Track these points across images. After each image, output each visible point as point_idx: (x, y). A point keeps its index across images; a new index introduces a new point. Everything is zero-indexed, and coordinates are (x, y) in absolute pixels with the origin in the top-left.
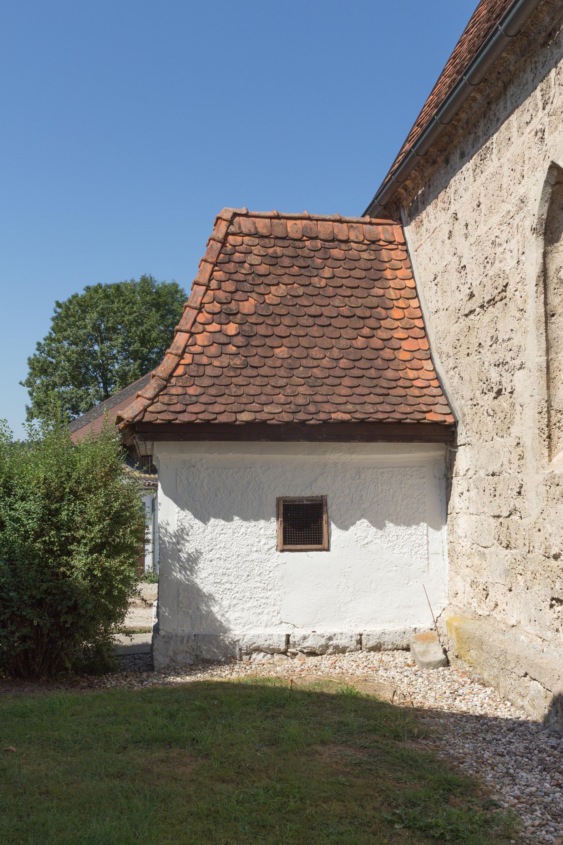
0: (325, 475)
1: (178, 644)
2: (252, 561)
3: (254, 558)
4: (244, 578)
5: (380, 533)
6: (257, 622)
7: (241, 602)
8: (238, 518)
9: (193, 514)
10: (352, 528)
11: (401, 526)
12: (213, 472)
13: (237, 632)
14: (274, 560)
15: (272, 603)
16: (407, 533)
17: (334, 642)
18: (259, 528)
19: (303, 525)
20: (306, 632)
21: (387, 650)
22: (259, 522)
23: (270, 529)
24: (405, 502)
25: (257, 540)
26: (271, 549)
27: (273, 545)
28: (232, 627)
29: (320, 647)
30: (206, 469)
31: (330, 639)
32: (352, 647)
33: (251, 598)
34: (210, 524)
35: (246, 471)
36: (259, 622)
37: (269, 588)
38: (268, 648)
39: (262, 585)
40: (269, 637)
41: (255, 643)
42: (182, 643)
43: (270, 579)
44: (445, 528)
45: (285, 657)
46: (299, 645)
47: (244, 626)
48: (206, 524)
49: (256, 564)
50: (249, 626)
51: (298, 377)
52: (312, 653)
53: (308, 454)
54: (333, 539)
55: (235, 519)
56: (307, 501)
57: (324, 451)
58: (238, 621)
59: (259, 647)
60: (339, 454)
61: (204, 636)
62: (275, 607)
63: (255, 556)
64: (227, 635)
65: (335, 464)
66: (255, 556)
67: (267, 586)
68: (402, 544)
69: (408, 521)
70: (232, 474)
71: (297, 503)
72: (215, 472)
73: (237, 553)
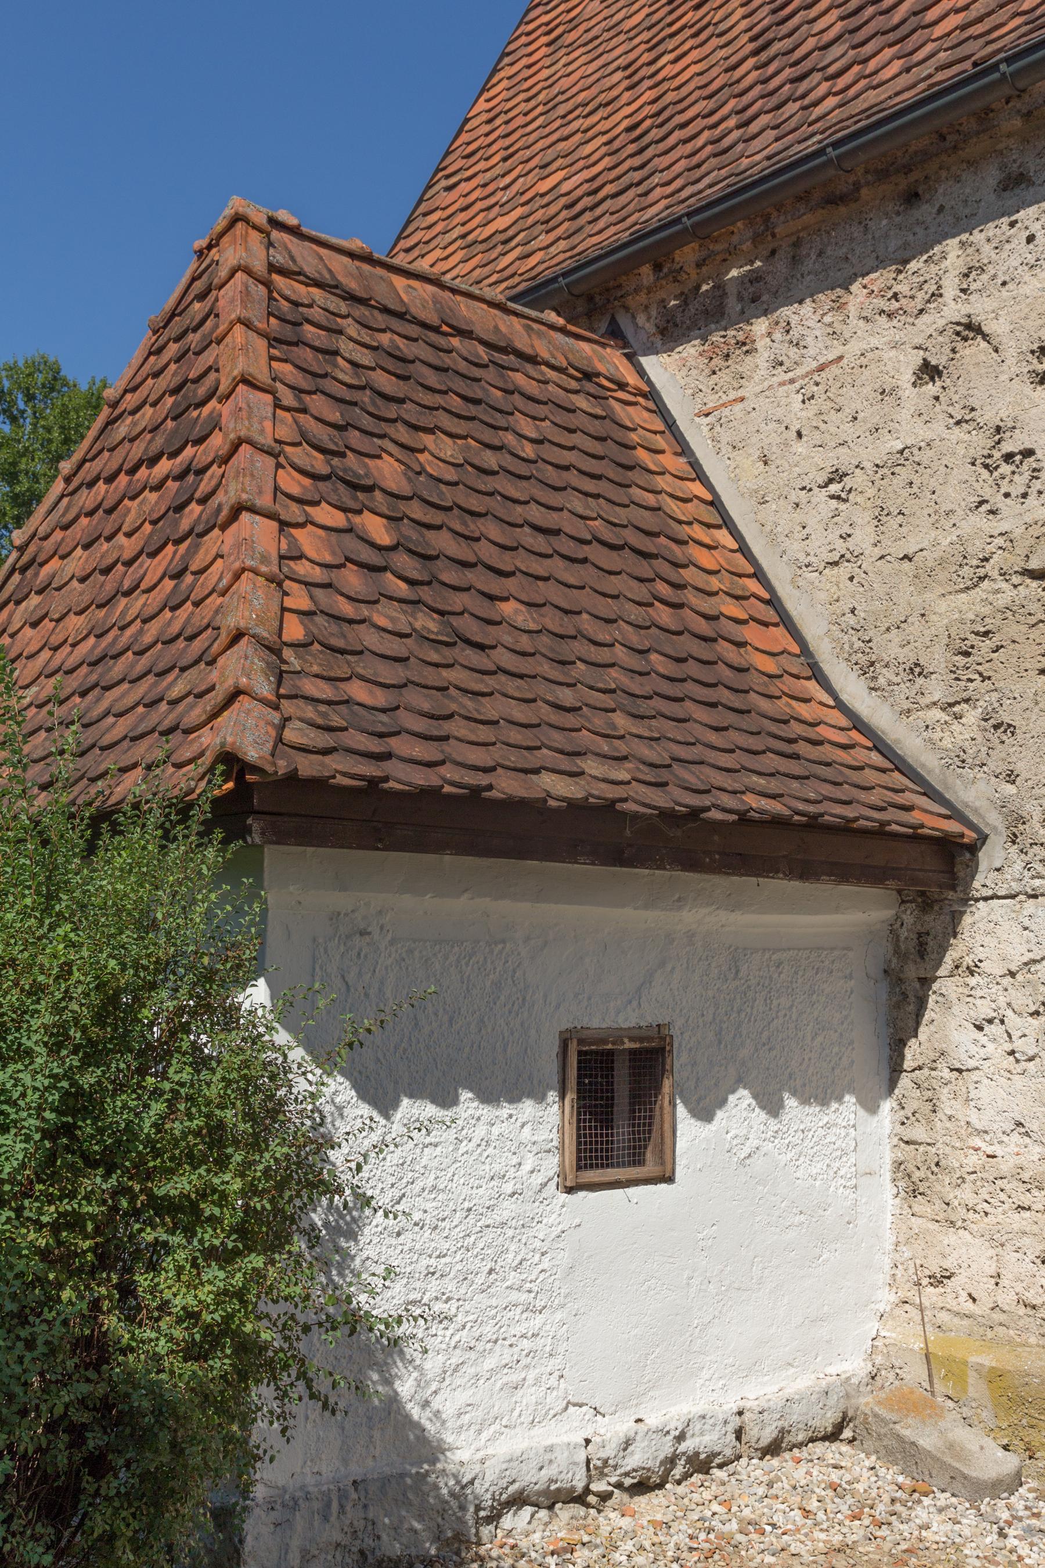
0: (669, 968)
1: (316, 1523)
2: (503, 1224)
3: (506, 1214)
4: (480, 1280)
5: (773, 1124)
6: (513, 1410)
7: (473, 1355)
8: (470, 1095)
9: (355, 1086)
10: (720, 1114)
11: (810, 1104)
12: (411, 951)
13: (462, 1455)
14: (552, 1219)
15: (548, 1349)
16: (821, 1124)
17: (688, 1445)
18: (519, 1124)
19: (619, 1108)
20: (623, 1426)
21: (794, 1446)
22: (521, 1105)
23: (538, 1127)
24: (820, 1039)
25: (515, 1160)
26: (546, 1184)
27: (551, 1173)
28: (449, 1438)
29: (662, 1463)
30: (392, 943)
31: (681, 1438)
32: (728, 1452)
33: (496, 1342)
34: (398, 1115)
35: (491, 952)
36: (516, 1413)
37: (539, 1304)
38: (546, 1492)
39: (523, 1297)
40: (548, 1456)
41: (514, 1481)
42: (326, 1518)
43: (542, 1276)
44: (887, 1106)
45: (582, 1511)
46: (615, 1467)
47: (479, 1432)
48: (387, 1117)
49: (510, 1233)
50: (492, 1428)
51: (591, 688)
52: (642, 1487)
53: (646, 907)
54: (681, 1145)
55: (462, 1099)
56: (632, 1039)
57: (679, 900)
58: (466, 1419)
59: (521, 1492)
60: (704, 911)
61: (385, 1481)
62: (552, 1361)
63: (508, 1209)
64: (439, 1466)
65: (691, 935)
66: (508, 1209)
67: (535, 1298)
68: (811, 1152)
69: (821, 1093)
70: (458, 961)
71: (610, 1046)
72: (416, 953)
73: (466, 1205)
